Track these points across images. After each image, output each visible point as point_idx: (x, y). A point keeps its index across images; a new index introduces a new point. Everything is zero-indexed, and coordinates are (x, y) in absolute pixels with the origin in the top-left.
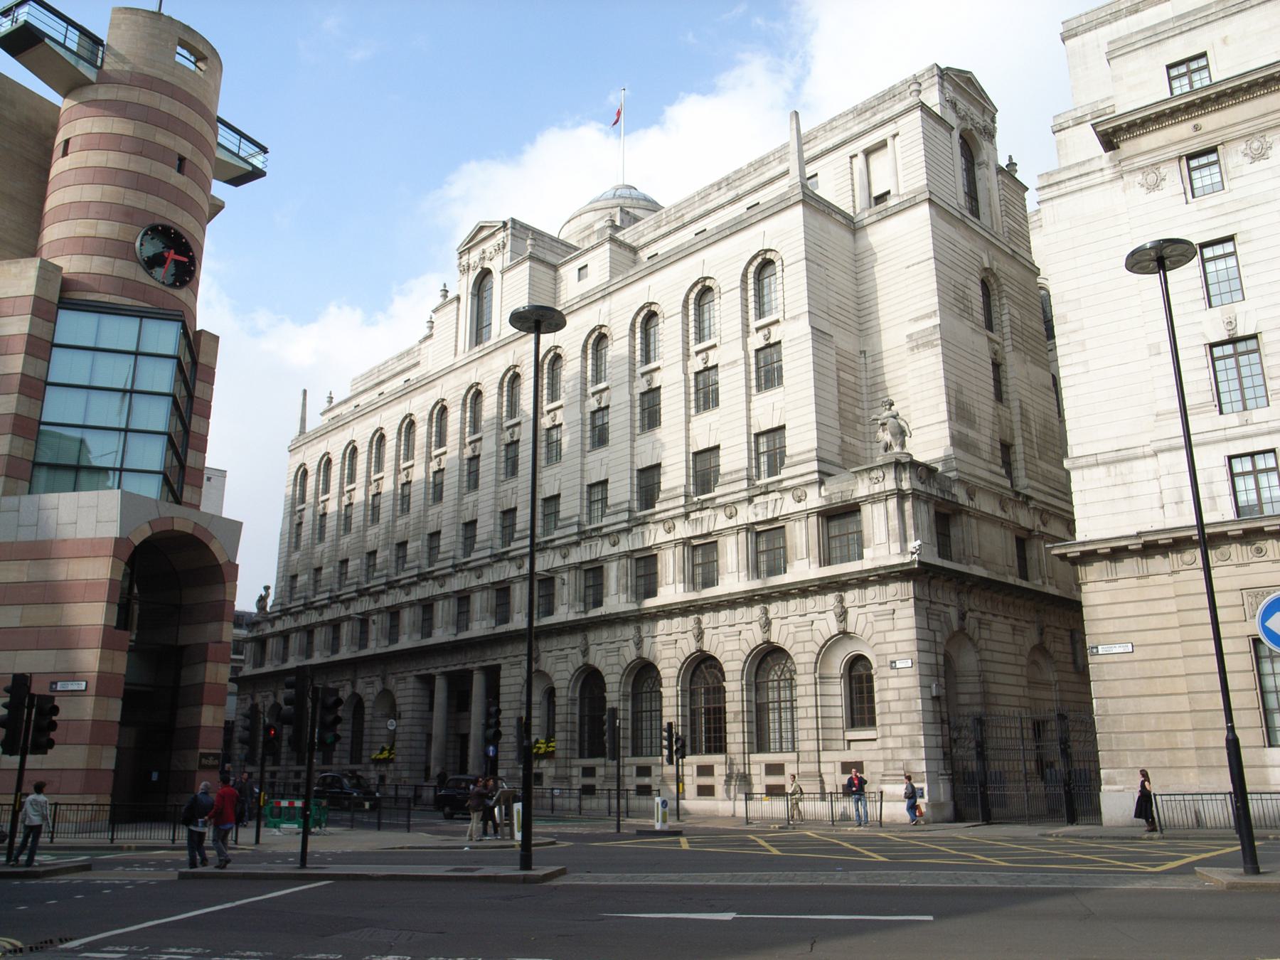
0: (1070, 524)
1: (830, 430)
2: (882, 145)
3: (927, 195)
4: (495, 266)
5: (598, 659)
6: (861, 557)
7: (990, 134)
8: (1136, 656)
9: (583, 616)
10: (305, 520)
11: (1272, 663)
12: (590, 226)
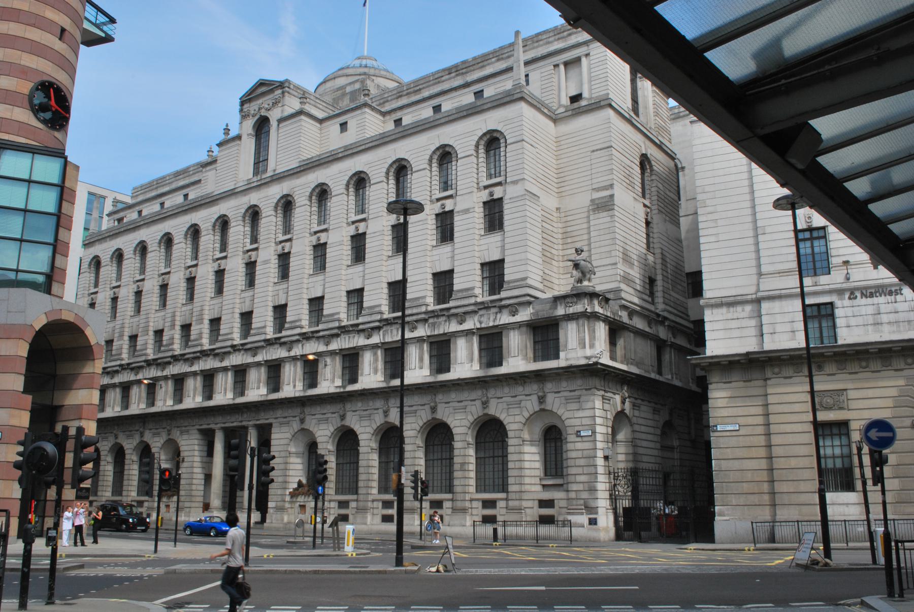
0: (700, 341)
2: (578, 60)
6: (557, 357)
8: (741, 433)
9: (342, 390)
11: (824, 439)
12: (343, 88)
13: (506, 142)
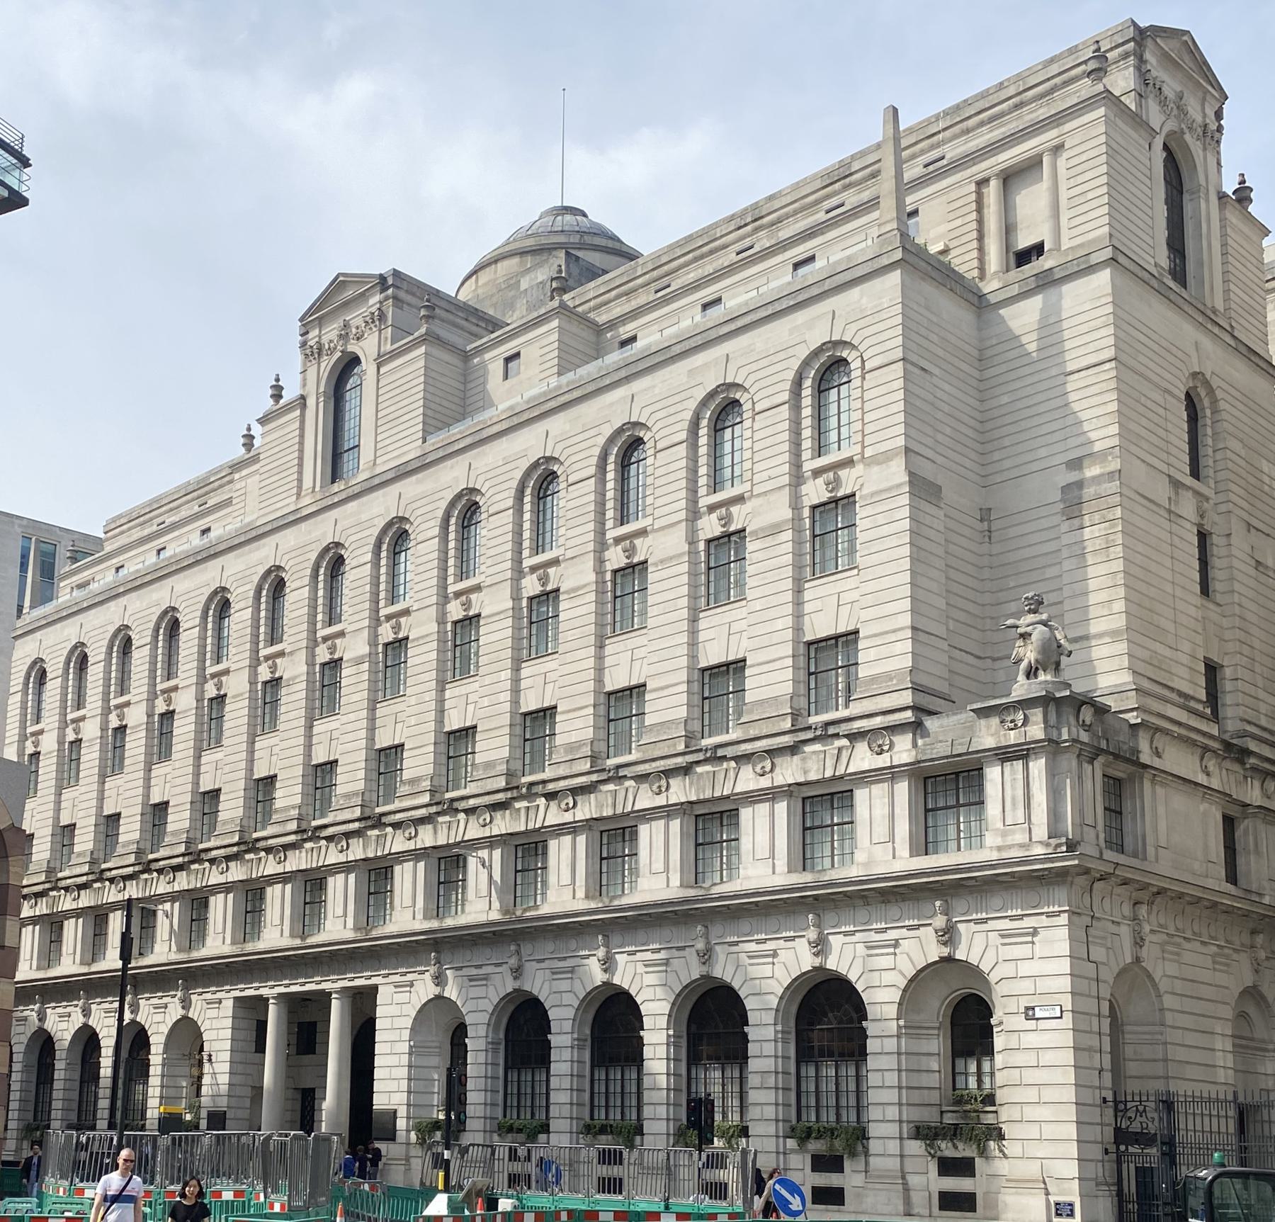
1: (933, 640)
3: (1108, 253)
4: (367, 348)
5: (539, 984)
7: (1212, 136)
10: (43, 748)
13: (863, 367)
